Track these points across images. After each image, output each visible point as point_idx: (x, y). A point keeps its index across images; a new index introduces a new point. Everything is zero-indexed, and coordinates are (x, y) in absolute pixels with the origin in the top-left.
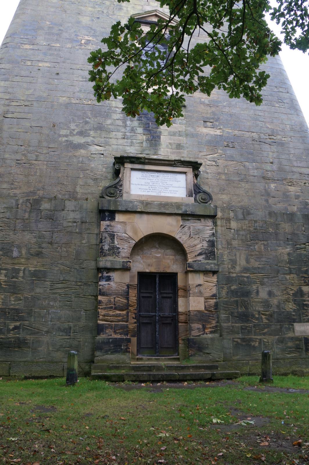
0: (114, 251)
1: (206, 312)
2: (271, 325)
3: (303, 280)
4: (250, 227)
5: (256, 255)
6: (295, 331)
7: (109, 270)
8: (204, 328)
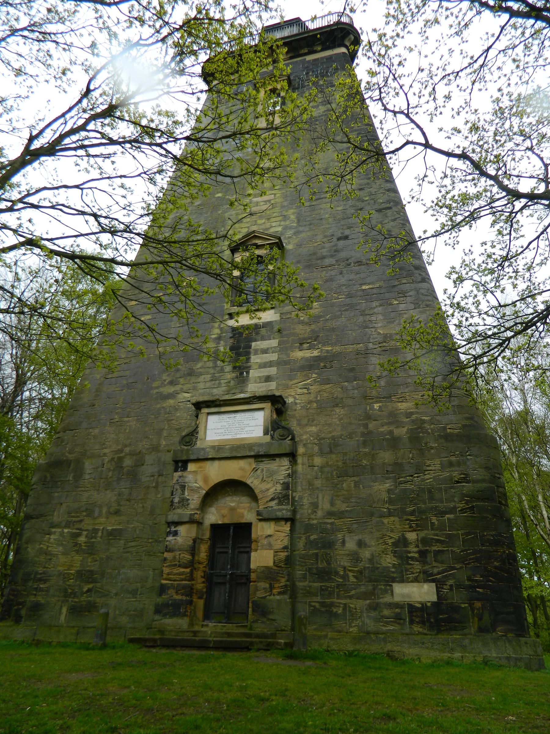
0: (184, 502)
1: (275, 568)
2: (360, 585)
3: (408, 524)
4: (337, 461)
5: (343, 495)
6: (395, 595)
7: (177, 524)
8: (271, 587)
